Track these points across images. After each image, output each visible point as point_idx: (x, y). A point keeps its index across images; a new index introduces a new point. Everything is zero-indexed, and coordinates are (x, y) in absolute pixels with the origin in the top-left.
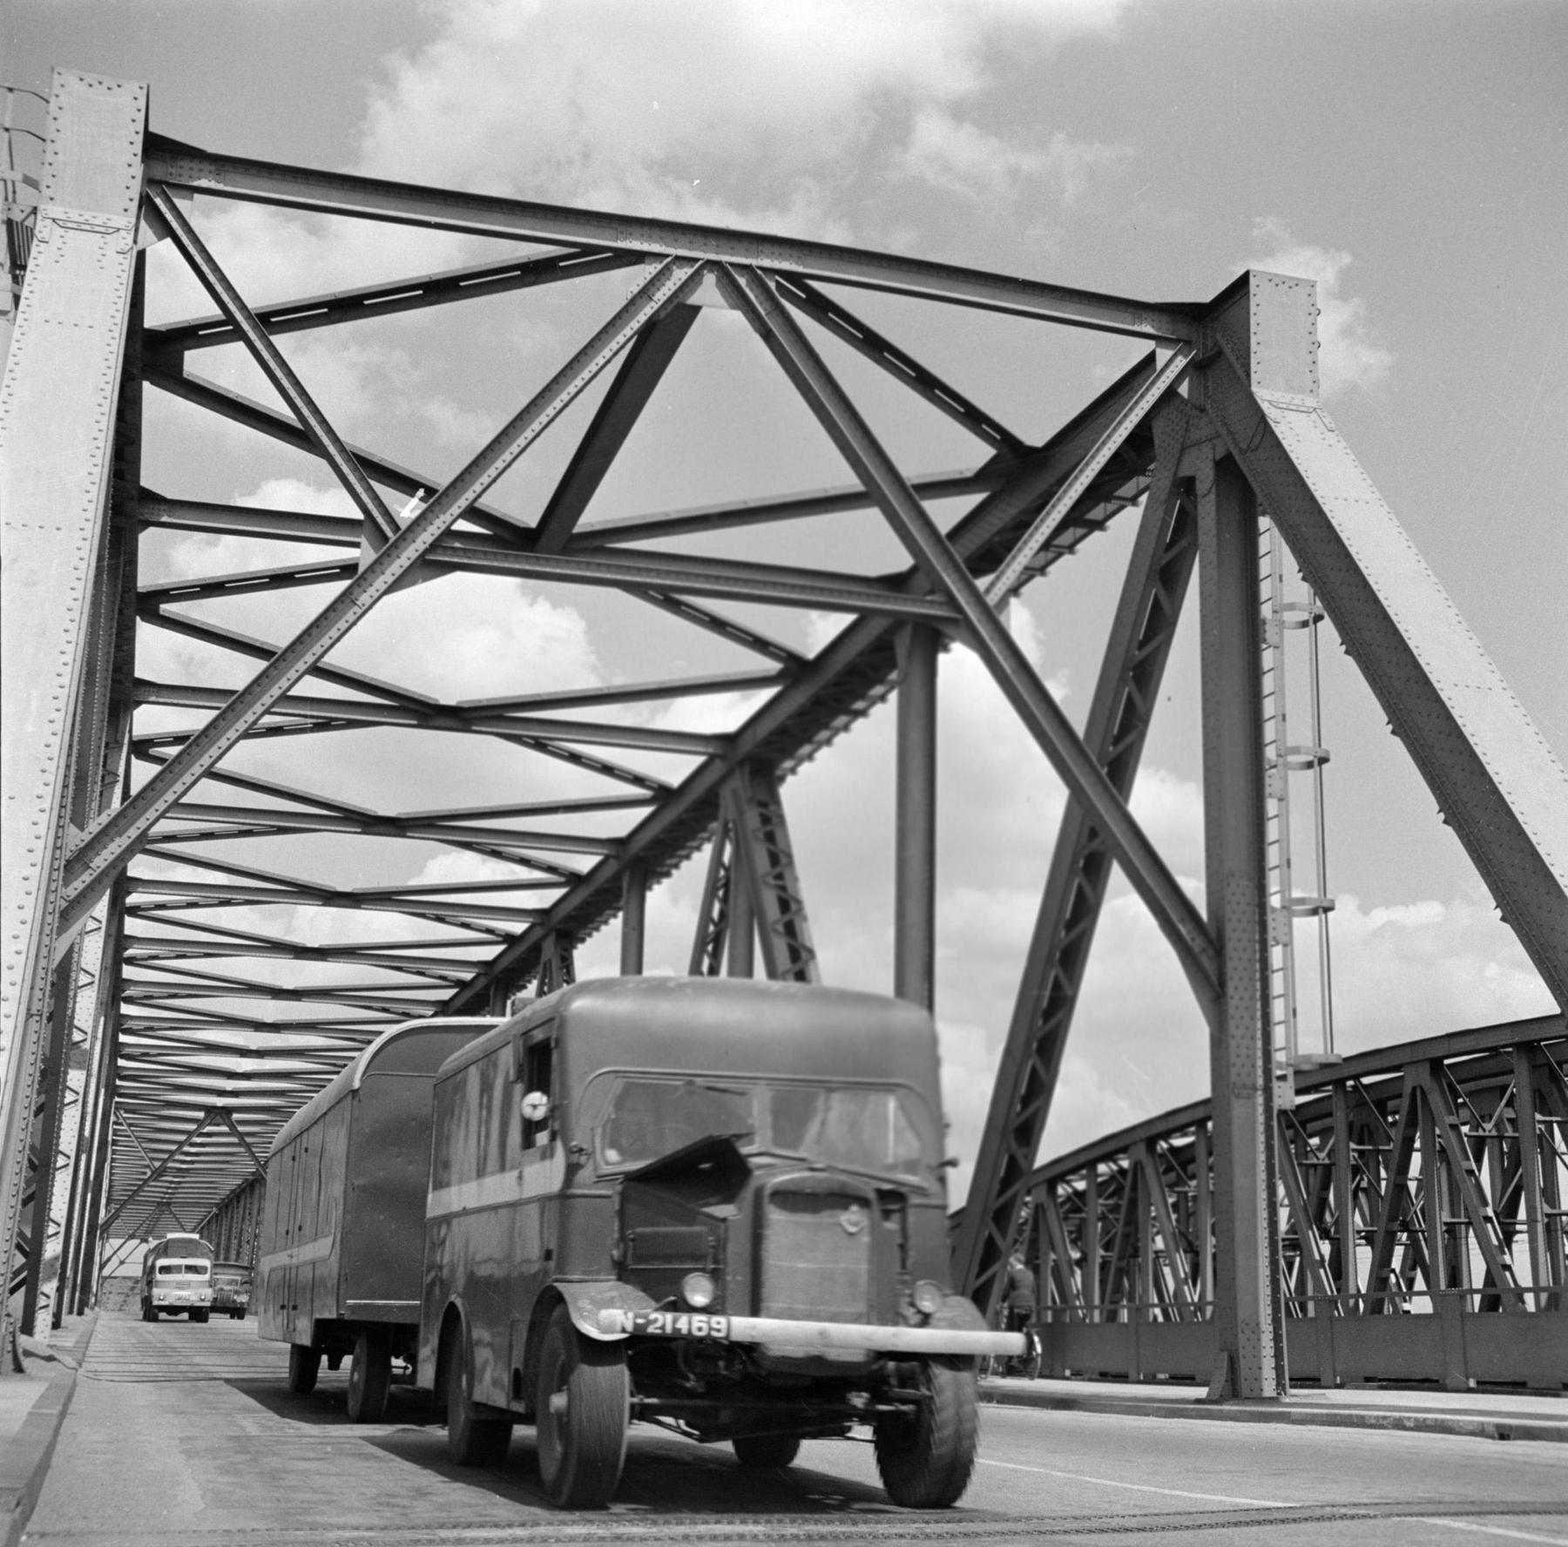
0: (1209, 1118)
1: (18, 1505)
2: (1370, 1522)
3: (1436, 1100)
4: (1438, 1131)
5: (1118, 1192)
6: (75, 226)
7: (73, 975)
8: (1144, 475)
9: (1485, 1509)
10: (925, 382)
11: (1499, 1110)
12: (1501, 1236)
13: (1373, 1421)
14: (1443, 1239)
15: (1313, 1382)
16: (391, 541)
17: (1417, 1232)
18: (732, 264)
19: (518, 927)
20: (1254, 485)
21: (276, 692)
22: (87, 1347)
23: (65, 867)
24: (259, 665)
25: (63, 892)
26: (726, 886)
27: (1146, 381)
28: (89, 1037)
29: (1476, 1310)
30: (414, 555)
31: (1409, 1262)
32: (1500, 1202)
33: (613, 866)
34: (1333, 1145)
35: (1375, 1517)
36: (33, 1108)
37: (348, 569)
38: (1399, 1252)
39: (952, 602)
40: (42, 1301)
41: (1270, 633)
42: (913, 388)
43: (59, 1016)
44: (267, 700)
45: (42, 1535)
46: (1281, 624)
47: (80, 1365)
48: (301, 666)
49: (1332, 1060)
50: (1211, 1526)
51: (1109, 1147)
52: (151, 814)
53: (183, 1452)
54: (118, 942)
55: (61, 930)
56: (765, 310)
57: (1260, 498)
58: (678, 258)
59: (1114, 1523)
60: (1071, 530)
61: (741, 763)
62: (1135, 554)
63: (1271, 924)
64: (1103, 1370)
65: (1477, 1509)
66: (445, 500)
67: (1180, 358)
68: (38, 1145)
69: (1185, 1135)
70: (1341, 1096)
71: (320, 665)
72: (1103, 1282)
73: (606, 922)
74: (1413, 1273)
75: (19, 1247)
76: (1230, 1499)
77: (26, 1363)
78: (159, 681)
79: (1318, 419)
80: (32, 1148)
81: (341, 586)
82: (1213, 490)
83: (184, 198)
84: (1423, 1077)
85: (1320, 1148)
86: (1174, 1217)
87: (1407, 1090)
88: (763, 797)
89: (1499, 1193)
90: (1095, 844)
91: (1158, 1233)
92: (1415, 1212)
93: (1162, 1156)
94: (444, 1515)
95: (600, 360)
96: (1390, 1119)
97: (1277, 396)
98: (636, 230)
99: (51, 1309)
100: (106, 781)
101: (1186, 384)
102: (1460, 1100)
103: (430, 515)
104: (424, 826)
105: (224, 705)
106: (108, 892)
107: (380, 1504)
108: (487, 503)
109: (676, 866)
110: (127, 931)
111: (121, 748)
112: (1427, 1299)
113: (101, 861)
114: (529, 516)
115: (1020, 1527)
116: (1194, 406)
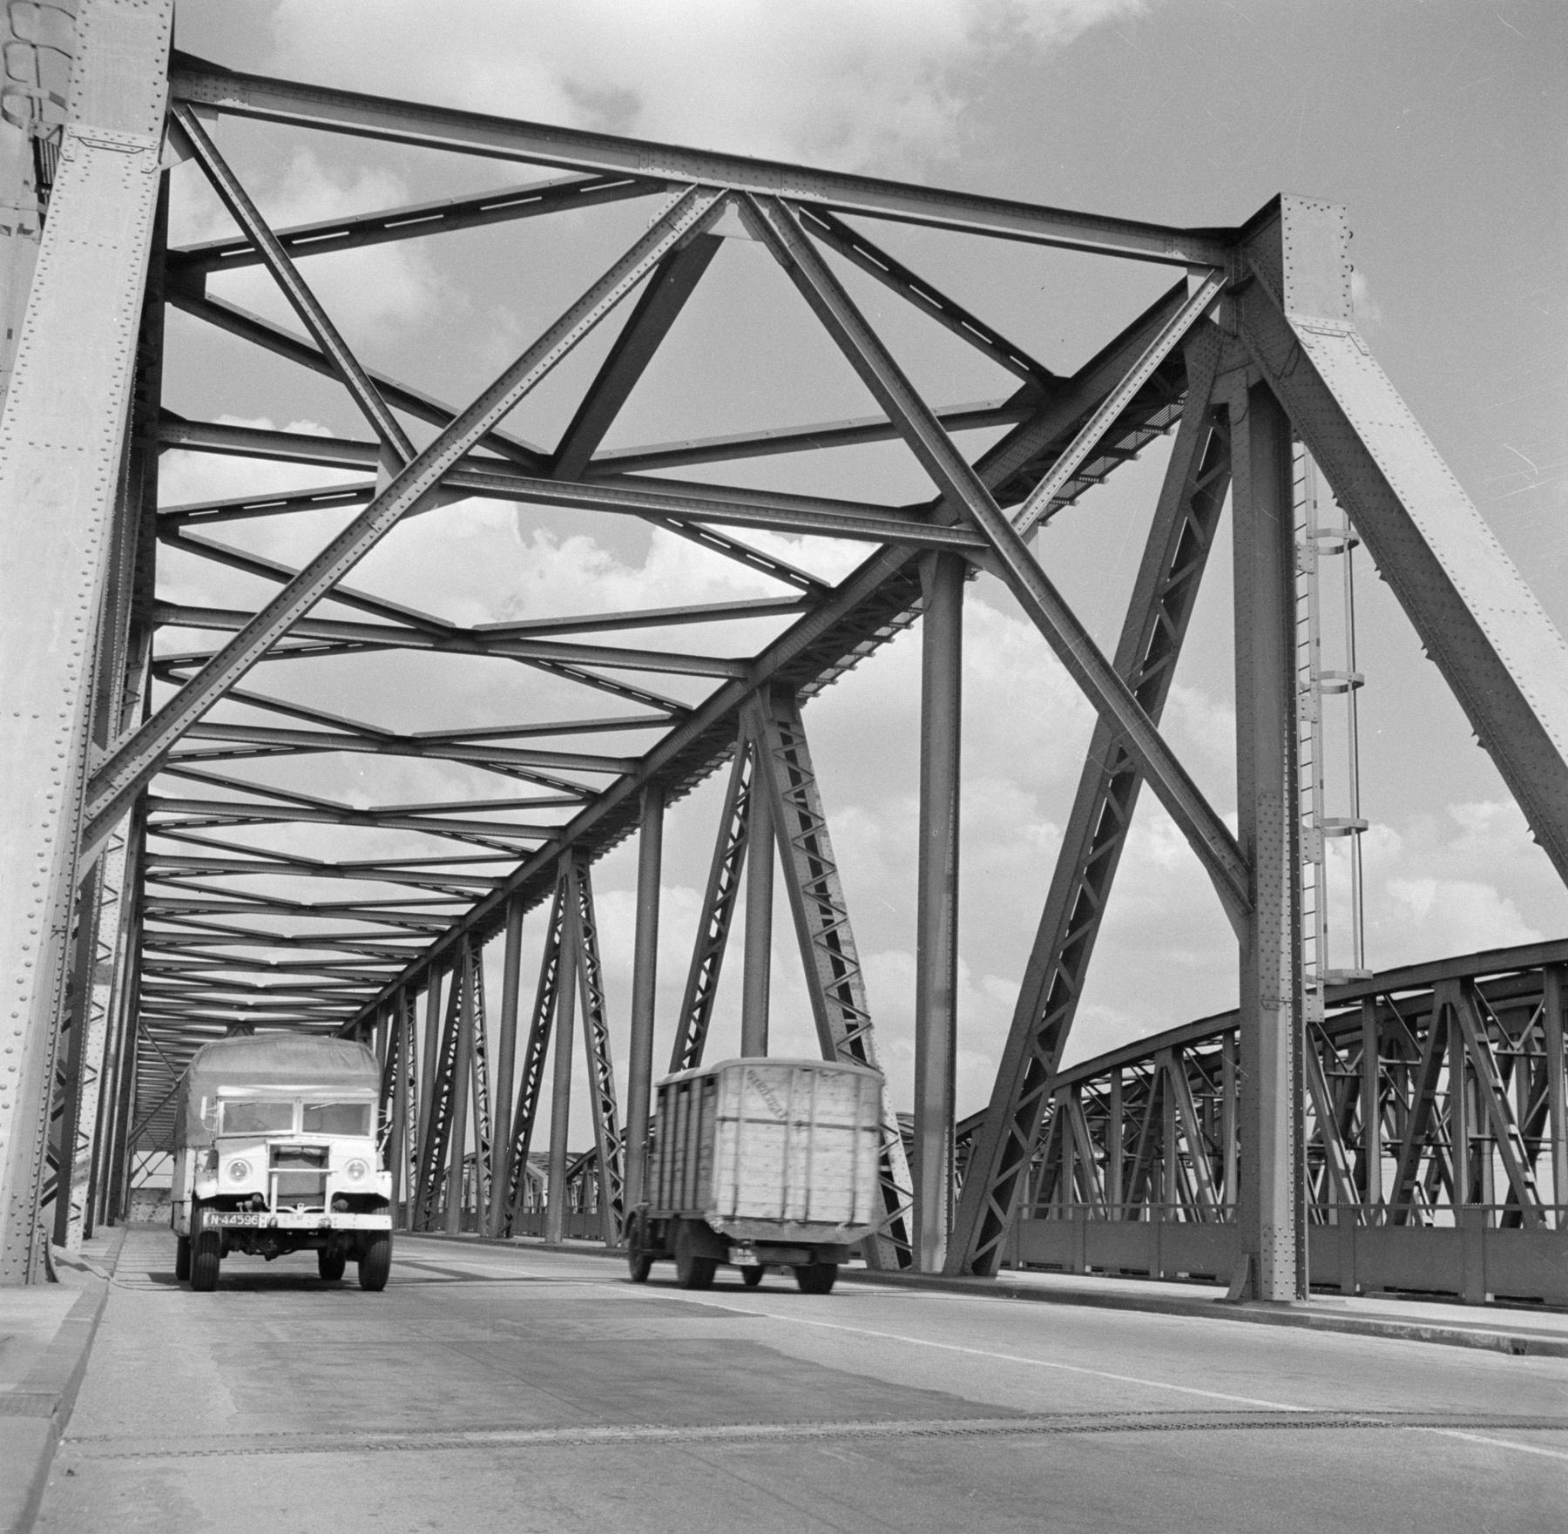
0: (1237, 1028)
1: (55, 1411)
2: (1382, 1431)
3: (1466, 1016)
4: (1466, 1048)
5: (1143, 1095)
6: (100, 144)
7: (97, 892)
8: (1176, 403)
9: (1495, 1422)
10: (952, 315)
11: (1528, 1029)
12: (1525, 1154)
13: (1391, 1331)
14: (1468, 1152)
15: (1333, 1288)
16: (408, 466)
17: (1441, 1145)
18: (756, 195)
19: (534, 845)
20: (1287, 411)
21: (293, 614)
22: (117, 1258)
23: (88, 786)
24: (276, 588)
25: (85, 810)
26: (746, 803)
27: (1177, 308)
28: (113, 953)
29: (1498, 1226)
30: (431, 481)
31: (1434, 1176)
32: (1529, 1112)
33: (630, 785)
34: (1362, 1058)
35: (1387, 1425)
36: (60, 1023)
37: (364, 493)
38: (1424, 1165)
39: (980, 532)
40: (73, 1212)
41: (1303, 559)
42: (941, 321)
43: (84, 936)
44: (284, 622)
45: (79, 1440)
46: (1316, 550)
47: (112, 1275)
48: (318, 589)
49: (1363, 975)
50: (1226, 1427)
51: (1136, 1053)
52: (171, 733)
53: (213, 1358)
54: (141, 862)
55: (84, 848)
56: (789, 241)
57: (1294, 424)
58: (700, 186)
59: (1130, 1420)
60: (1101, 459)
61: (762, 686)
62: (1152, 537)
63: (1302, 844)
64: (1123, 1267)
65: (1490, 1422)
66: (461, 426)
67: (1212, 284)
68: (66, 1060)
69: (1212, 1043)
70: (1371, 1010)
71: (336, 588)
72: (1125, 1182)
73: (623, 839)
74: (1436, 1187)
75: (49, 1160)
76: (1245, 1400)
77: (59, 1272)
78: (179, 603)
79: (1351, 343)
80: (60, 1062)
81: (358, 509)
82: (1247, 416)
83: (210, 118)
84: (1454, 994)
85: (1349, 1060)
86: (1199, 1121)
87: (1438, 1006)
88: (787, 719)
89: (1524, 1113)
90: (1124, 764)
91: (1182, 1136)
92: (1442, 1127)
93: (1187, 1062)
94: (470, 1418)
95: (620, 289)
96: (1419, 1035)
97: (1310, 321)
98: (658, 157)
99: (83, 1220)
100: (128, 701)
101: (1217, 310)
102: (1490, 1018)
103: (446, 441)
104: (441, 745)
105: (242, 628)
106: (129, 811)
107: (409, 1408)
108: (503, 429)
109: (695, 784)
110: (149, 849)
111: (142, 667)
112: (1450, 1212)
113: (123, 779)
114: (546, 442)
115: (1038, 1424)
116: (1226, 333)
